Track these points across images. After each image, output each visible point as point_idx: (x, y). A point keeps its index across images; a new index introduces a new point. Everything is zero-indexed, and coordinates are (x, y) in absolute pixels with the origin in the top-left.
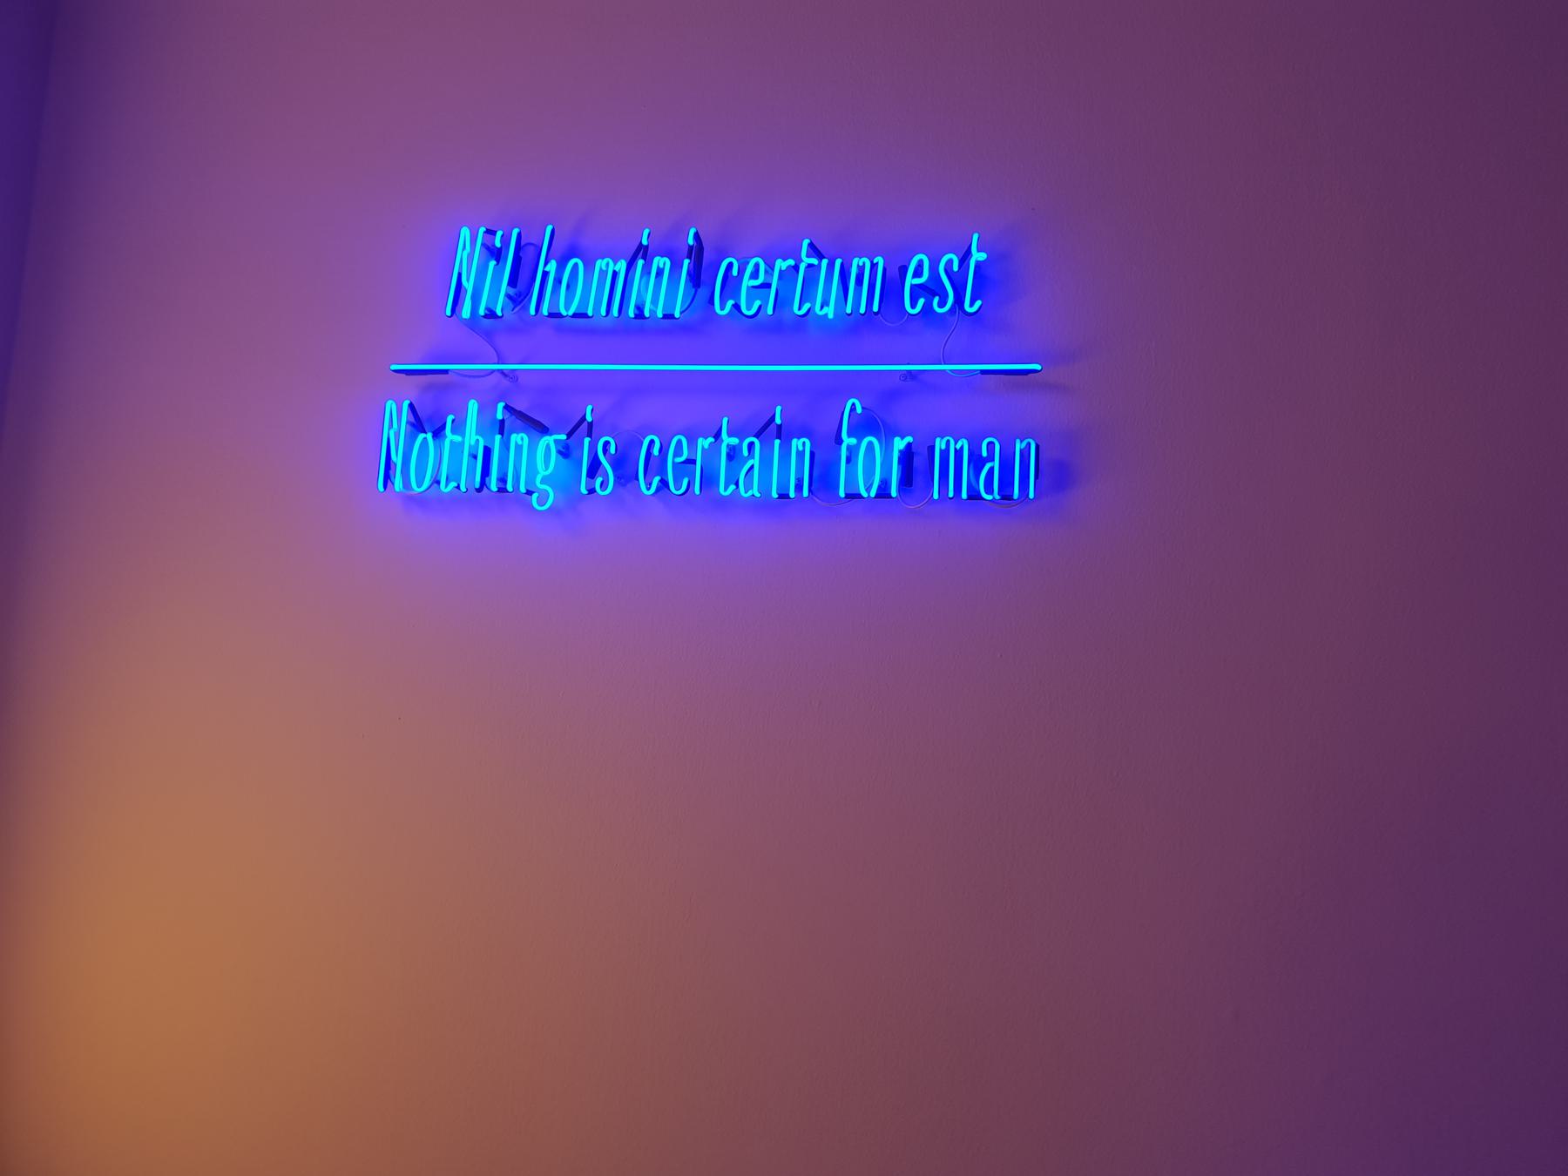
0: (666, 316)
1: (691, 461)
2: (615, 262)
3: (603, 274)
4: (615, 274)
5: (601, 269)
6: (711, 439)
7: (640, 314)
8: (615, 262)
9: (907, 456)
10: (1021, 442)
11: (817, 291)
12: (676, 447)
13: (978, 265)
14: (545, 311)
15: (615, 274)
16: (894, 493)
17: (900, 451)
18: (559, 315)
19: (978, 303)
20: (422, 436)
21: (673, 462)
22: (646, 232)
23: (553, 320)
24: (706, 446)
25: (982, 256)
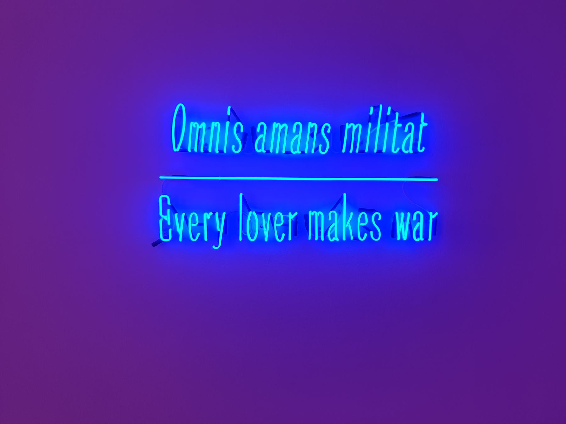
0: (286, 152)
1: (201, 224)
2: (200, 124)
3: (194, 129)
4: (200, 130)
5: (193, 127)
6: (211, 213)
7: (206, 150)
8: (200, 124)
9: (295, 222)
10: (433, 214)
11: (240, 138)
12: (251, 218)
13: (424, 127)
14: (357, 151)
15: (200, 130)
16: (206, 239)
17: (433, 219)
18: (290, 153)
19: (424, 149)
20: (250, 213)
21: (192, 227)
22: (229, 108)
23: (287, 155)
24: (209, 218)
25: (426, 124)
